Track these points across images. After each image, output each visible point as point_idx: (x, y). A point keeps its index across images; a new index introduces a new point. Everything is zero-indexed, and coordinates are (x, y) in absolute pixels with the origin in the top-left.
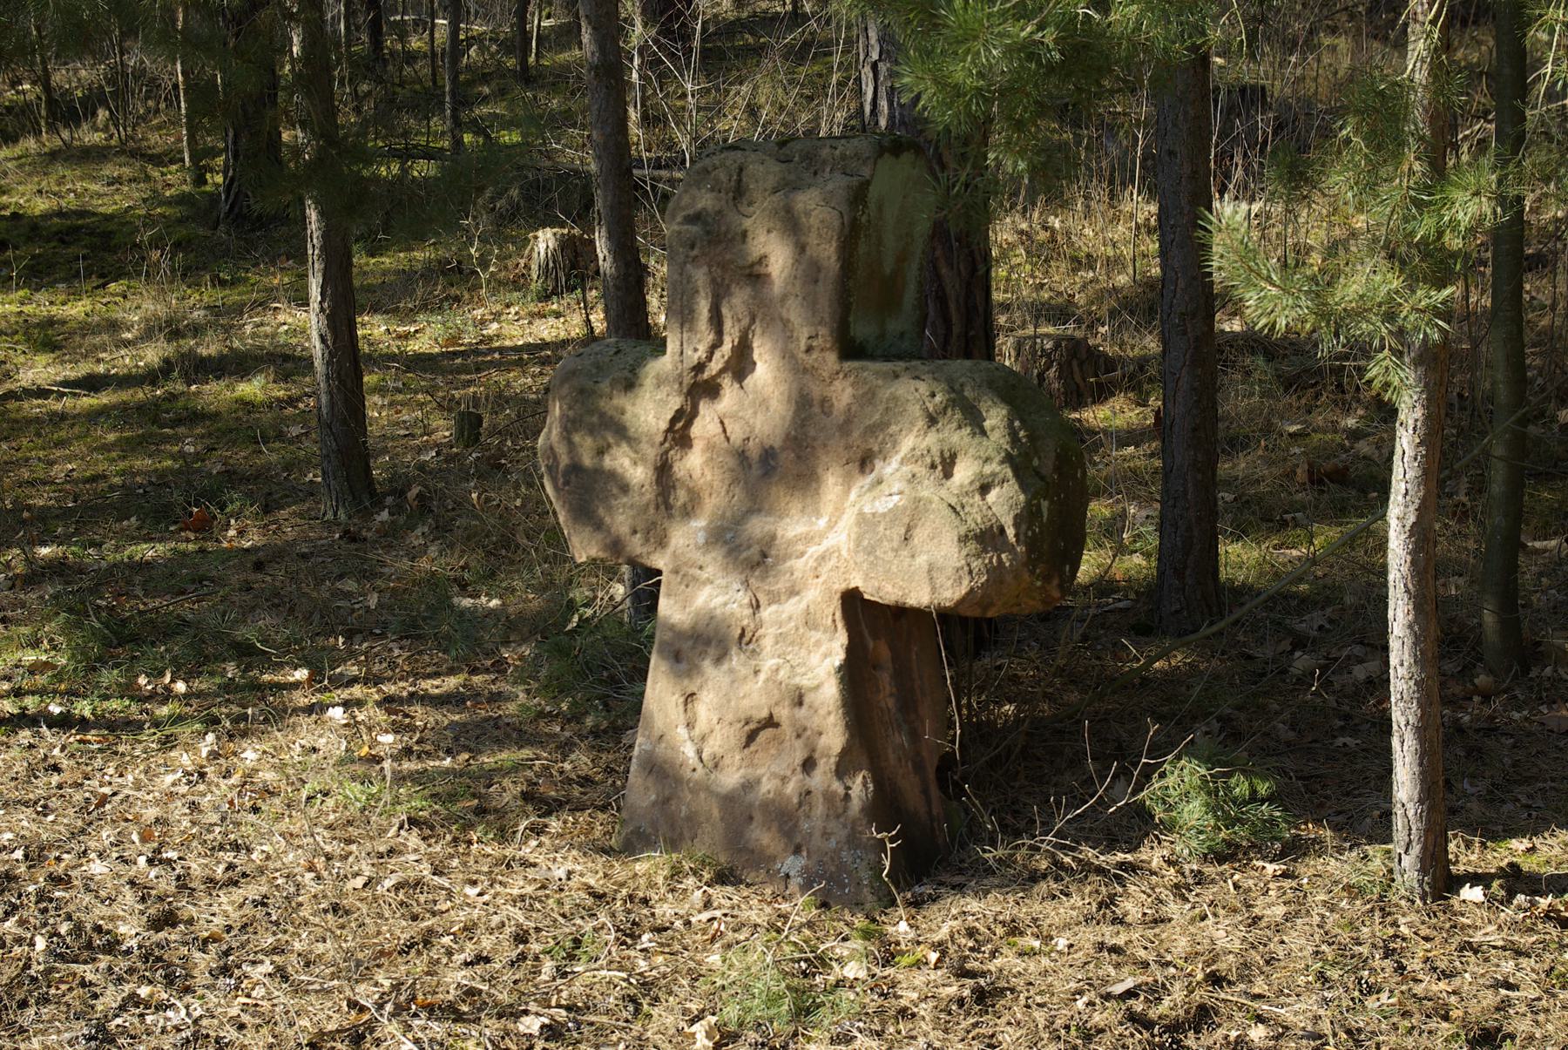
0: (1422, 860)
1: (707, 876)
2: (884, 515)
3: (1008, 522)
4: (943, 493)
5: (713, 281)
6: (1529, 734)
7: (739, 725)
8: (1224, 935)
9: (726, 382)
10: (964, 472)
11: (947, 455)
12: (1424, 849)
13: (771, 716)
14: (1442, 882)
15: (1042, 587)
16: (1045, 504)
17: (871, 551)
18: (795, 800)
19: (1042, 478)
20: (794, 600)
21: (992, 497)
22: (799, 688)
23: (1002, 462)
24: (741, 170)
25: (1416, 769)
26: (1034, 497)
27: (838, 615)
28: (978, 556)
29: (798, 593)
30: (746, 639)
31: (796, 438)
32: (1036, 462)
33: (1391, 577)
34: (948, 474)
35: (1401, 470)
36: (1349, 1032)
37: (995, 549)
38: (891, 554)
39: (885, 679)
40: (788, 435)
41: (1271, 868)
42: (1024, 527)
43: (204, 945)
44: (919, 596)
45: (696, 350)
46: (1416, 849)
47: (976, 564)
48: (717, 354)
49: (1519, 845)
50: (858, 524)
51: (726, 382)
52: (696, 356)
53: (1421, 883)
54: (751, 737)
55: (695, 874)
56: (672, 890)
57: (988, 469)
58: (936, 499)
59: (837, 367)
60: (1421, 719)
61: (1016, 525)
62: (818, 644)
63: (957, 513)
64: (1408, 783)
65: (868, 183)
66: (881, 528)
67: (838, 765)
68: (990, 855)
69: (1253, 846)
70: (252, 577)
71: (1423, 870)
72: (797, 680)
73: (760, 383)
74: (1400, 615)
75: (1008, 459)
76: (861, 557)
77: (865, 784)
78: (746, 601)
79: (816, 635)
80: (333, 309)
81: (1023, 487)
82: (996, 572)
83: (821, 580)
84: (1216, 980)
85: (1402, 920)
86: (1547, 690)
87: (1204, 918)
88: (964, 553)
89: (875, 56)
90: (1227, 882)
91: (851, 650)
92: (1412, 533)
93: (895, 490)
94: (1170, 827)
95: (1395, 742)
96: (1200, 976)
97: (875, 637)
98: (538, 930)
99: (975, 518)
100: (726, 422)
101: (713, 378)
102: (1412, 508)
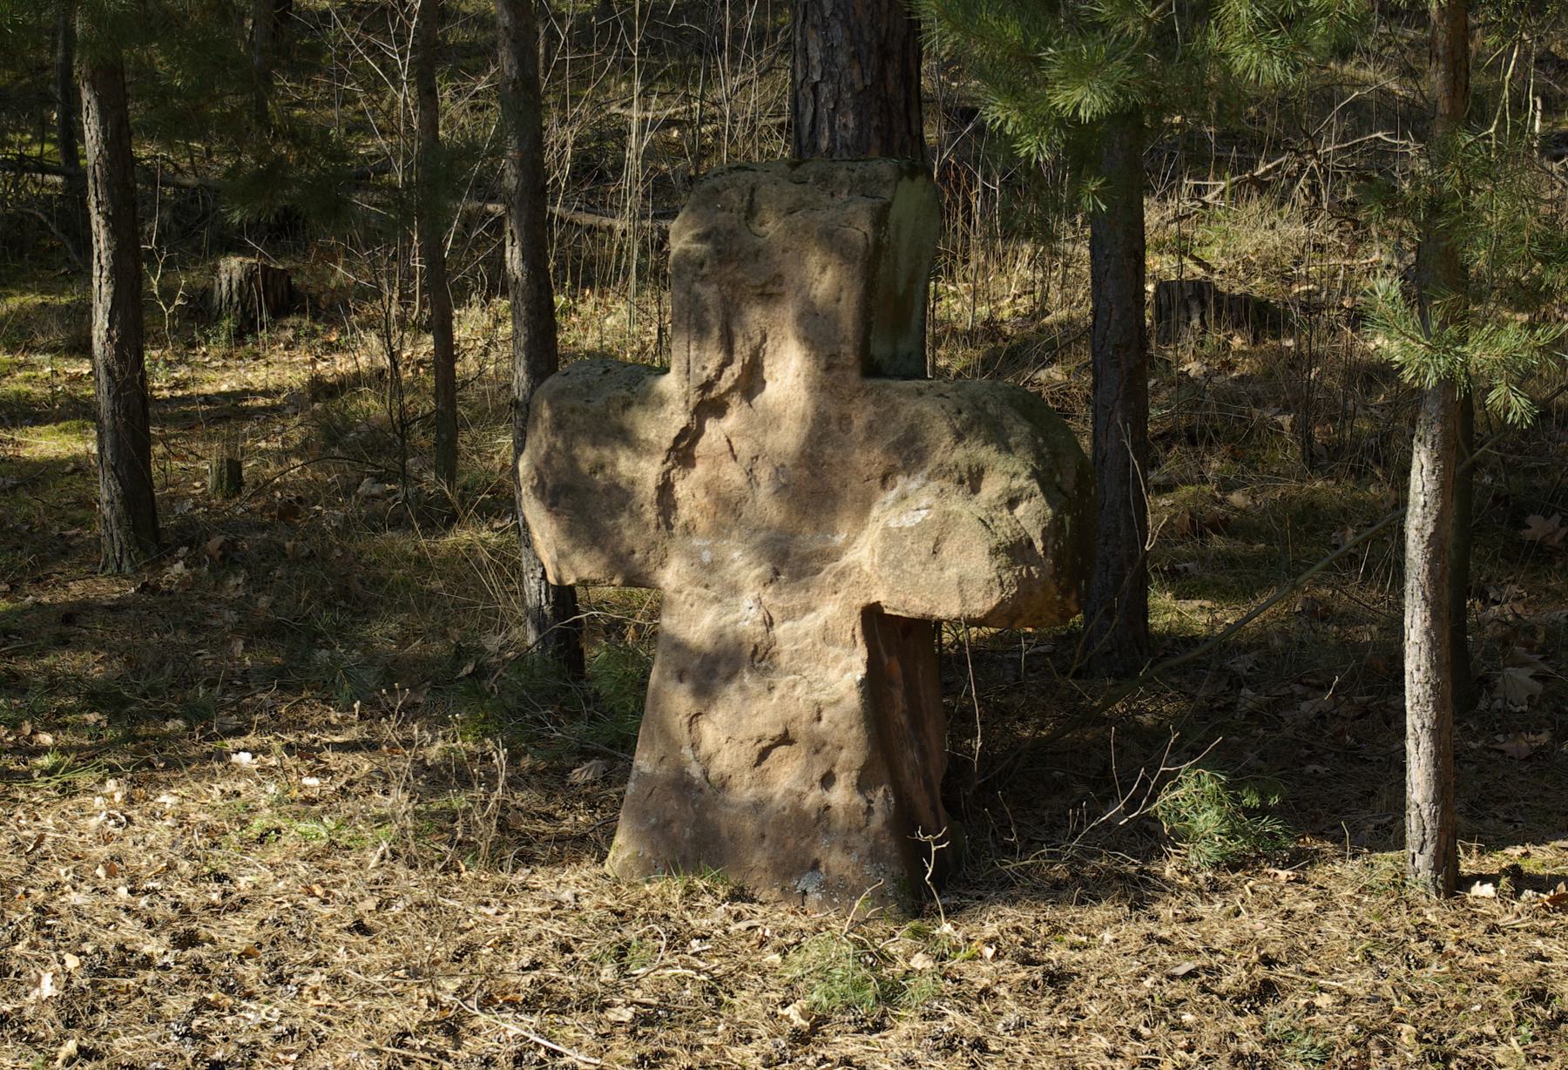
0: (1435, 858)
1: (722, 894)
2: (911, 529)
3: (1036, 535)
4: (972, 506)
5: (724, 299)
6: (1490, 761)
7: (751, 744)
8: (1260, 925)
9: (735, 400)
10: (992, 487)
11: (975, 470)
12: (1438, 848)
13: (786, 732)
14: (1454, 884)
15: (1062, 601)
16: (1068, 518)
17: (897, 565)
18: (813, 816)
19: (1065, 494)
20: (812, 615)
21: (1020, 510)
22: (817, 703)
23: (1029, 478)
24: (753, 190)
25: (1431, 770)
26: (1060, 512)
27: (858, 630)
28: (1008, 568)
29: (814, 610)
30: (759, 657)
31: (811, 456)
32: (1058, 478)
33: (1408, 586)
34: (975, 490)
35: (1419, 483)
36: (1411, 995)
37: (1025, 563)
38: (918, 568)
39: (898, 694)
40: (802, 453)
41: (1283, 875)
42: (1051, 540)
43: (244, 957)
44: (948, 607)
45: (704, 368)
46: (1430, 848)
47: (1006, 576)
48: (727, 372)
49: (1516, 851)
50: (884, 539)
51: (735, 400)
52: (705, 374)
53: (1434, 880)
54: (764, 755)
55: (710, 892)
56: (689, 909)
57: (1016, 484)
58: (966, 512)
59: (858, 385)
60: (1436, 722)
61: (1044, 538)
62: (837, 659)
63: (988, 527)
64: (1423, 784)
65: (889, 205)
66: (908, 542)
67: (859, 778)
68: (1011, 866)
69: (1260, 856)
70: (65, 630)
71: (1436, 869)
72: (816, 696)
73: (771, 401)
74: (1417, 622)
75: (1034, 474)
76: (885, 572)
77: (886, 797)
78: (760, 618)
79: (834, 651)
80: (122, 337)
81: (1051, 502)
82: (1024, 583)
83: (840, 595)
84: (1268, 961)
85: (1426, 911)
86: (1498, 721)
87: (1238, 913)
88: (995, 565)
89: (816, 78)
90: (1248, 885)
91: (873, 664)
92: (1430, 543)
93: (923, 504)
94: (1180, 836)
95: (1410, 745)
96: (1255, 958)
97: (889, 654)
98: (577, 941)
99: (1005, 530)
100: (733, 440)
101: (721, 396)
102: (1430, 520)
